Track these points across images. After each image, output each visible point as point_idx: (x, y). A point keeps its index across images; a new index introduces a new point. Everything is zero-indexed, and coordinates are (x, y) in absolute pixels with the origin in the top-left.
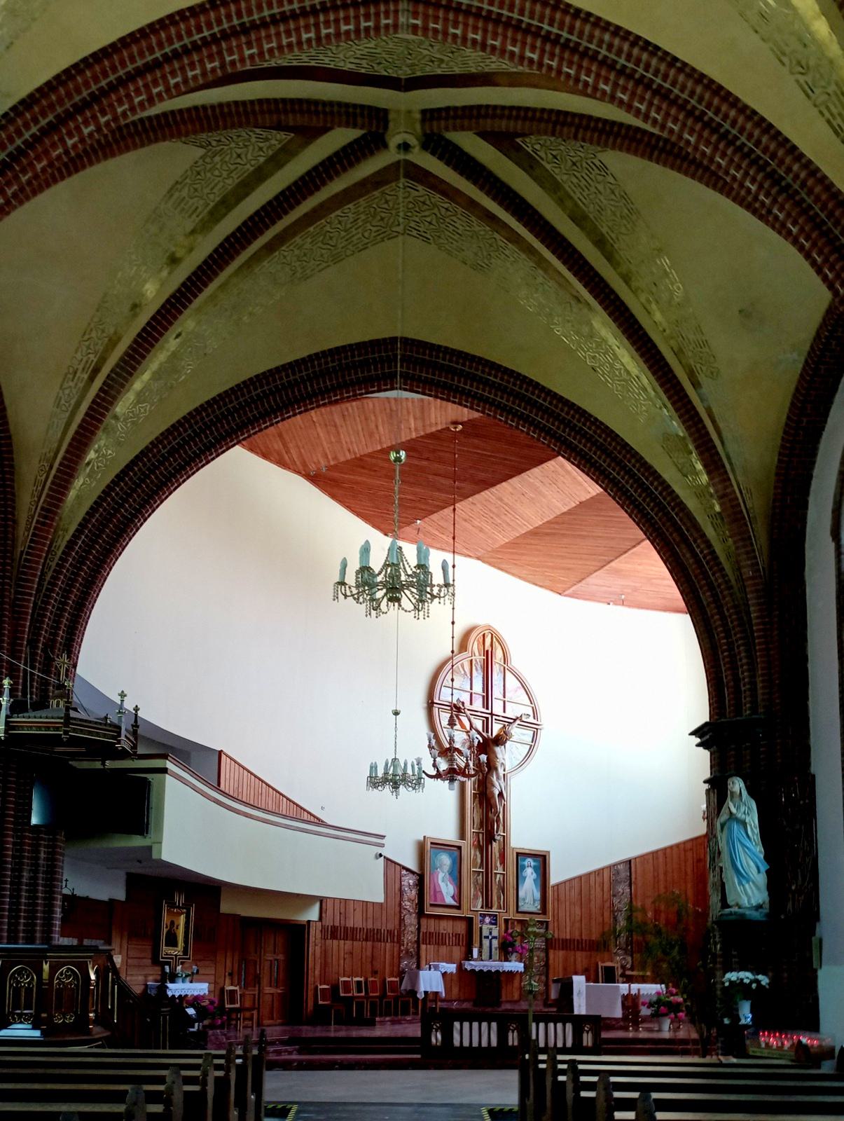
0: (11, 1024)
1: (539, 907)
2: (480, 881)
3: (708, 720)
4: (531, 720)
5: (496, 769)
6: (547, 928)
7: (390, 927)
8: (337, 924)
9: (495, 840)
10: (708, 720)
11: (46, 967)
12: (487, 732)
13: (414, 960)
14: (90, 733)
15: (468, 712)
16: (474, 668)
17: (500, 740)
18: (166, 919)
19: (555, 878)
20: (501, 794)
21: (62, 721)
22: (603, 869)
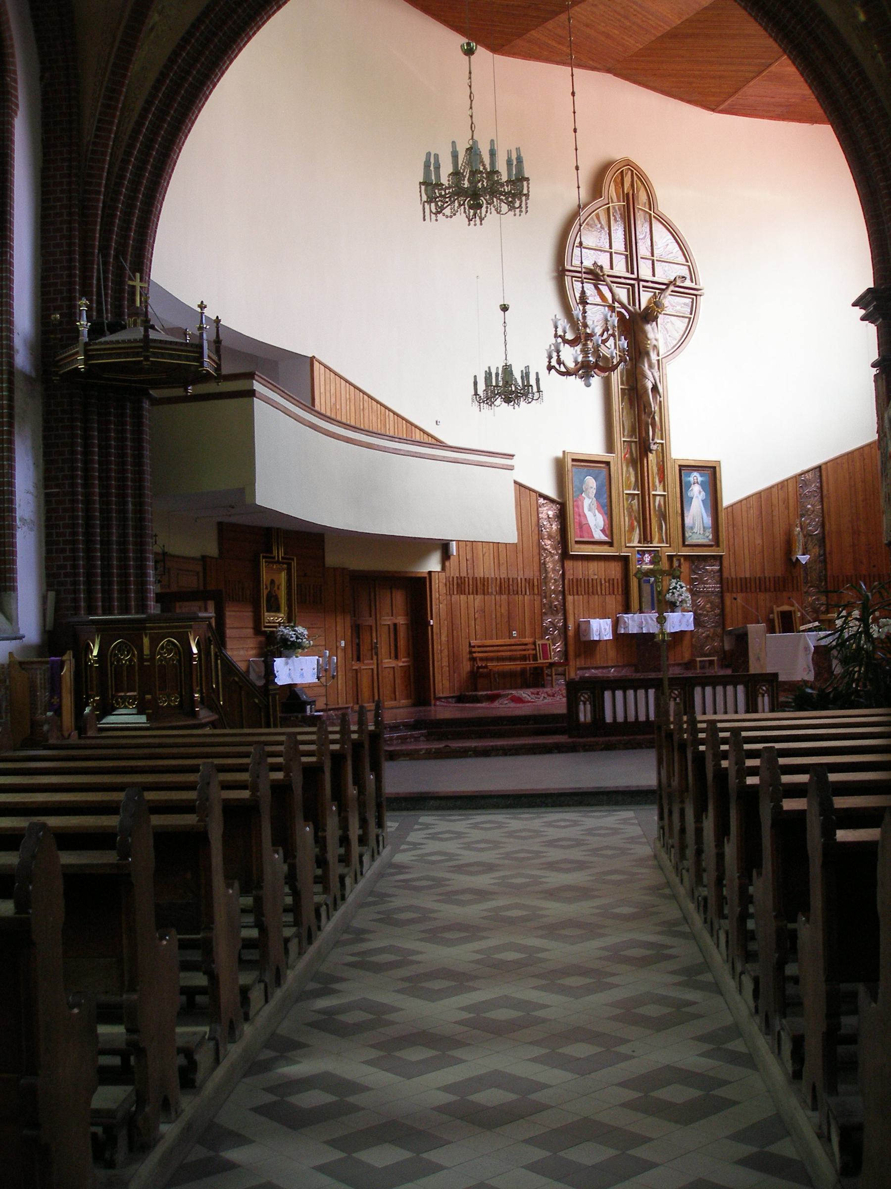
0: (115, 709)
1: (711, 537)
2: (635, 507)
3: (872, 286)
4: (688, 283)
5: (648, 354)
6: (721, 565)
7: (529, 574)
8: (464, 574)
9: (651, 451)
10: (872, 286)
11: (146, 641)
12: (634, 304)
13: (560, 616)
14: (171, 357)
15: (609, 279)
16: (612, 218)
17: (649, 315)
18: (265, 577)
19: (730, 496)
20: (655, 388)
21: (142, 344)
22: (787, 480)
